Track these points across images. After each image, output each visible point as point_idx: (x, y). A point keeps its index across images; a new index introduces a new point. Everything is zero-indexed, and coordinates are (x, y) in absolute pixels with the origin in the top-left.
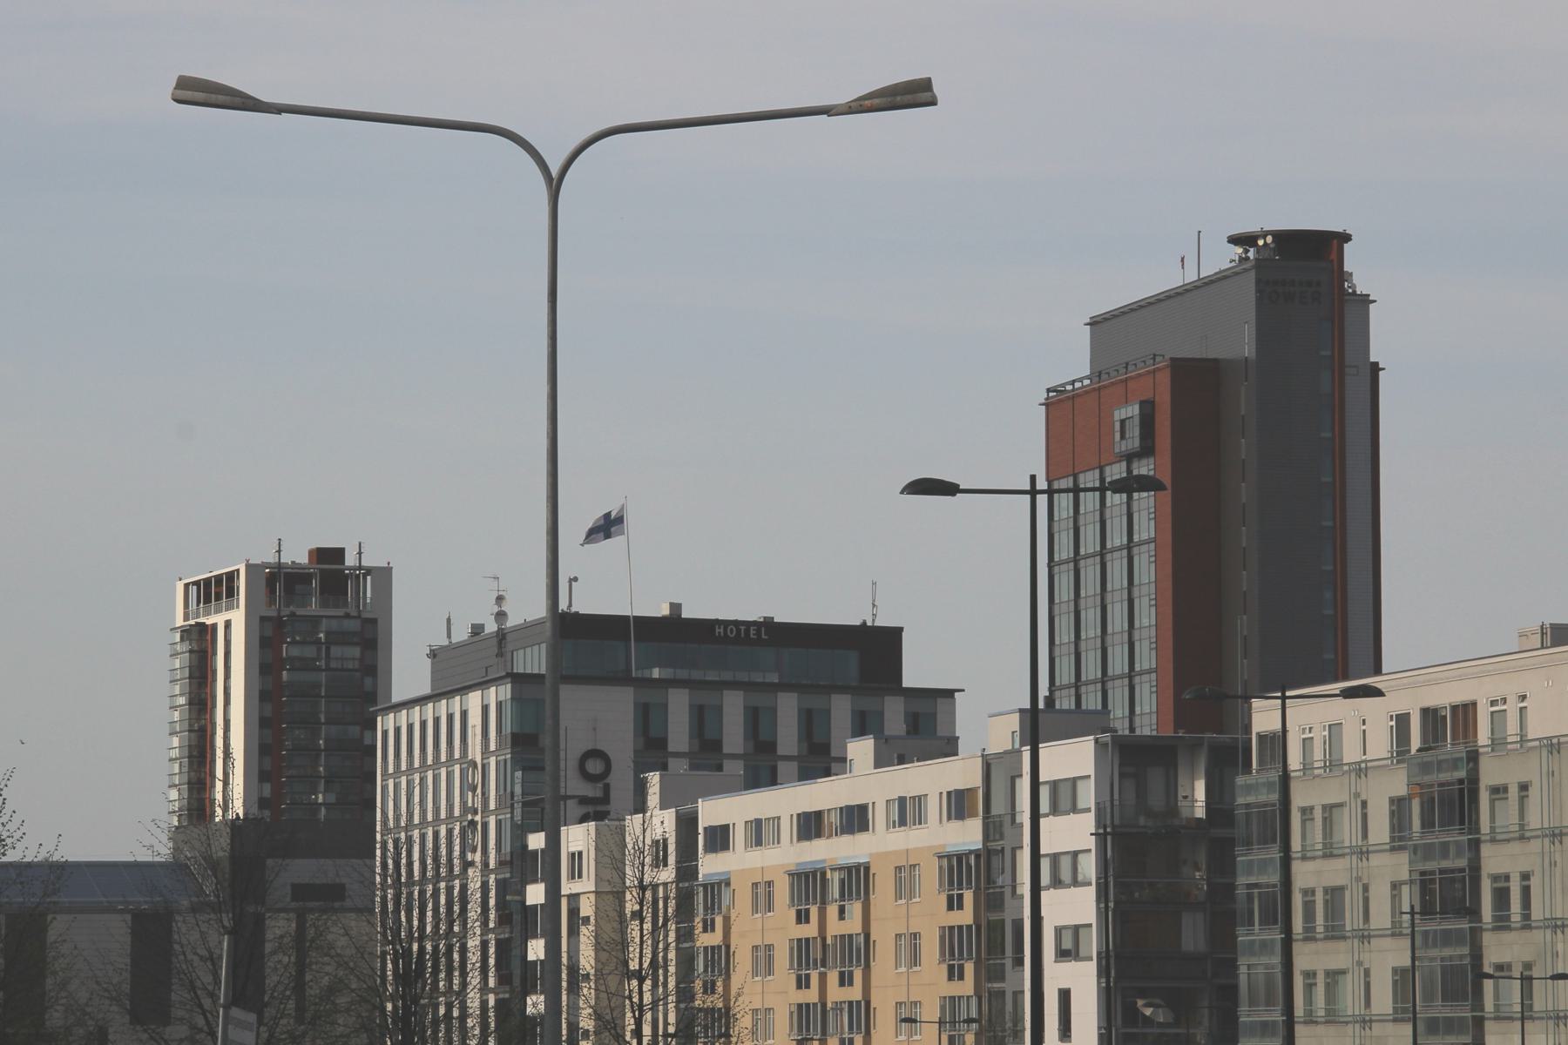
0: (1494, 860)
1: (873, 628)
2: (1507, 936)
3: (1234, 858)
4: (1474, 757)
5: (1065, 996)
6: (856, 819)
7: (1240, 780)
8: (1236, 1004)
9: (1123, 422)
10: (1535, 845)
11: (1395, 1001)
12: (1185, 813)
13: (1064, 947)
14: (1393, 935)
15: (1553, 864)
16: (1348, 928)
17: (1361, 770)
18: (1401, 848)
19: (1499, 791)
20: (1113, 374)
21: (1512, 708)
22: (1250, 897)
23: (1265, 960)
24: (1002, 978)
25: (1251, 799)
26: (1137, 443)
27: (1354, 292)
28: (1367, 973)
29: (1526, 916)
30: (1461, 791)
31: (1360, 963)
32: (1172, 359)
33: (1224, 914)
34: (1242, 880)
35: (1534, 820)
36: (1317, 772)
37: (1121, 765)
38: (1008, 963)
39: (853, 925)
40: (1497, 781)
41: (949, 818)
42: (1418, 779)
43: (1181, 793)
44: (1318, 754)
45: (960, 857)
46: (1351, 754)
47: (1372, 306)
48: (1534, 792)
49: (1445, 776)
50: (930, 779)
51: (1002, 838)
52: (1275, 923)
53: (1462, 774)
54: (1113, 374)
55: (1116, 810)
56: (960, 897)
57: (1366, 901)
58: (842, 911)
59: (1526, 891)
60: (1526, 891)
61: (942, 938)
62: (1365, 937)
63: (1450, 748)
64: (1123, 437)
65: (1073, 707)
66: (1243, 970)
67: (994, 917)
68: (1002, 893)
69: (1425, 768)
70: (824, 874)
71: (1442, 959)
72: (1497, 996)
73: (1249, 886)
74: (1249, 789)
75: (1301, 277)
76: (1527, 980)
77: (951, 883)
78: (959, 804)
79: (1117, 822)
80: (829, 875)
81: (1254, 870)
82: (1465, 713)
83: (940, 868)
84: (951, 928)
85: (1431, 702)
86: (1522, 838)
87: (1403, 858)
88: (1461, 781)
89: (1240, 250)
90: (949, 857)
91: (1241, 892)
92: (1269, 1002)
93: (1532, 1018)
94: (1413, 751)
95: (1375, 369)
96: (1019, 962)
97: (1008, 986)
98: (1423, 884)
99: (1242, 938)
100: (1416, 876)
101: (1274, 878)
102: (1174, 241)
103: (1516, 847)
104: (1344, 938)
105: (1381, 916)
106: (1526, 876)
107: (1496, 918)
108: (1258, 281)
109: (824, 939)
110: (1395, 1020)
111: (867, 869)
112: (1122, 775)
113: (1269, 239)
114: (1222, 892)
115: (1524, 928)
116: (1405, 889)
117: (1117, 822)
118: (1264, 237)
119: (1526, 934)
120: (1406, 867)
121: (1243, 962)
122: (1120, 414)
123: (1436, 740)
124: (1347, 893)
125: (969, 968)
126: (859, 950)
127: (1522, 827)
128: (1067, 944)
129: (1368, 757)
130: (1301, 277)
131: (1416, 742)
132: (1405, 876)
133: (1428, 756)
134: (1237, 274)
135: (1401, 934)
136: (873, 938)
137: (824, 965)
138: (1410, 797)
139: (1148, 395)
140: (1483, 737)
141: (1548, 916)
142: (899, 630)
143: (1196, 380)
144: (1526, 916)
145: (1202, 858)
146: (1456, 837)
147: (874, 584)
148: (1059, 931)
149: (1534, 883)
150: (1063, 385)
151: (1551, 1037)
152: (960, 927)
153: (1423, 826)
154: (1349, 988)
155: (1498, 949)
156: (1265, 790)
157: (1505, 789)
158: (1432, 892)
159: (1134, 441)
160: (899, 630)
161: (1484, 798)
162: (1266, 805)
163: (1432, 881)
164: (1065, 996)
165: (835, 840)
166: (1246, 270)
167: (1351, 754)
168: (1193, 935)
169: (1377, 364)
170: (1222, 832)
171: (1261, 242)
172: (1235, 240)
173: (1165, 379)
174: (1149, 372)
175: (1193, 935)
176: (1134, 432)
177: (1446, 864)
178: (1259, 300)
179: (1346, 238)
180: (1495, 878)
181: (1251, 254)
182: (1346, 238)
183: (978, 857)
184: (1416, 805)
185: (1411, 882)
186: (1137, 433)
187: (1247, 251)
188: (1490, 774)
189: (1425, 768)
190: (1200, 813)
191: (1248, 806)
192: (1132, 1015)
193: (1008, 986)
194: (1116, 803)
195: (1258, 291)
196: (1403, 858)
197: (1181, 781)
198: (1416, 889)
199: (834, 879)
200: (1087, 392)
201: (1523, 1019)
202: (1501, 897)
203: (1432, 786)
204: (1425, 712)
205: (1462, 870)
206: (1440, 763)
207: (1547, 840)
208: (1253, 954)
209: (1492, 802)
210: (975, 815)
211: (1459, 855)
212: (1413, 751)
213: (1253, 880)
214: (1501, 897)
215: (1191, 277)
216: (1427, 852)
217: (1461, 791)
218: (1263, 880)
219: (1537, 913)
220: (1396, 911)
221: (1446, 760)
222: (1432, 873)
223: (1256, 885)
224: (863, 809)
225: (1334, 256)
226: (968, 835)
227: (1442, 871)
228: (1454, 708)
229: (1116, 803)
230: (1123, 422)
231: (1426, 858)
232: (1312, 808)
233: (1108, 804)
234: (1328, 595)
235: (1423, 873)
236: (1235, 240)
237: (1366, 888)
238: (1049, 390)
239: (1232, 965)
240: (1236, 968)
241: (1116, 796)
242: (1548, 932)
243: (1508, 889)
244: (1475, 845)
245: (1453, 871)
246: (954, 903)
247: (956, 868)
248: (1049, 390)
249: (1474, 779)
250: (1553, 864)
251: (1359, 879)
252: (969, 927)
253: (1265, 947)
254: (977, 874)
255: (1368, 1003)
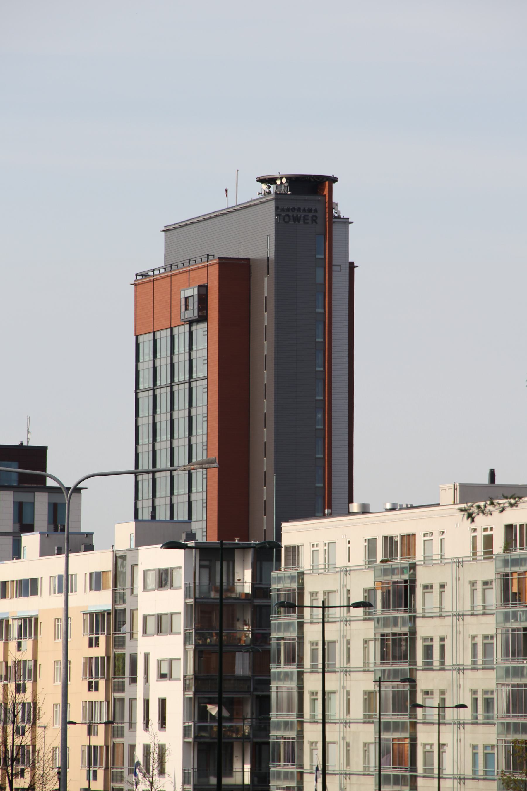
0: (425, 629)
1: (28, 447)
2: (430, 674)
3: (270, 621)
4: (413, 567)
5: (163, 703)
6: (29, 587)
7: (274, 574)
8: (268, 710)
9: (186, 299)
10: (448, 620)
11: (365, 711)
12: (238, 590)
13: (162, 672)
14: (364, 671)
15: (458, 632)
16: (337, 666)
17: (347, 571)
18: (369, 619)
19: (427, 587)
20: (180, 266)
21: (436, 538)
22: (279, 645)
23: (287, 684)
24: (123, 690)
25: (280, 586)
26: (196, 314)
27: (339, 216)
28: (348, 693)
29: (442, 663)
30: (406, 587)
31: (344, 687)
32: (219, 258)
33: (262, 654)
34: (274, 635)
35: (448, 607)
36: (320, 571)
37: (200, 560)
38: (127, 681)
39: (27, 655)
40: (427, 582)
41: (91, 589)
42: (381, 579)
43: (237, 577)
44: (321, 560)
45: (97, 614)
46: (341, 561)
47: (350, 226)
48: (448, 589)
49: (397, 578)
50: (83, 564)
51: (124, 602)
52: (294, 661)
53: (406, 577)
54: (180, 266)
55: (197, 588)
56: (97, 639)
57: (349, 650)
58: (19, 645)
59: (442, 647)
60: (442, 647)
61: (85, 664)
62: (347, 672)
63: (399, 562)
64: (186, 309)
65: (168, 518)
66: (273, 690)
67: (119, 651)
68: (124, 637)
69: (385, 572)
70: (7, 621)
71: (393, 687)
72: (424, 604)
73: (279, 639)
74: (279, 579)
75: (305, 203)
76: (442, 707)
77: (91, 630)
78: (96, 581)
79: (197, 596)
80: (11, 622)
81: (281, 628)
82: (409, 540)
83: (84, 620)
84: (91, 658)
85: (389, 534)
86: (441, 616)
87: (371, 625)
88: (406, 581)
89: (264, 186)
90: (91, 614)
91: (273, 642)
92: (289, 710)
93: (444, 724)
94: (378, 562)
95: (352, 266)
96: (134, 680)
97: (126, 695)
98: (382, 640)
99: (274, 669)
100: (379, 637)
101: (293, 634)
102: (224, 176)
103: (437, 621)
104: (335, 672)
105: (357, 661)
106: (442, 639)
107: (426, 664)
108: (277, 208)
109: (7, 663)
110: (364, 723)
111: (36, 619)
112: (200, 566)
113: (284, 180)
114: (261, 637)
115: (441, 670)
116: (372, 644)
117: (197, 596)
118: (281, 179)
119: (442, 673)
120: (372, 631)
121: (274, 685)
122: (185, 294)
123: (391, 555)
124: (337, 645)
125: (102, 684)
126: (30, 671)
127: (441, 609)
128: (165, 670)
129: (351, 564)
130: (305, 203)
131: (380, 556)
132: (372, 636)
133: (387, 565)
134: (262, 203)
135: (369, 671)
136: (39, 663)
137: (6, 679)
138: (375, 589)
139: (203, 282)
140: (419, 556)
141: (455, 663)
142: (45, 448)
143: (235, 273)
144: (442, 663)
145: (249, 618)
146: (402, 614)
147: (29, 418)
148: (159, 663)
149: (448, 643)
150: (147, 272)
151: (455, 735)
152: (97, 658)
153: (383, 607)
154: (337, 702)
155: (425, 681)
156: (289, 581)
157: (432, 587)
158: (387, 646)
159: (194, 312)
160: (45, 448)
161: (419, 591)
162: (289, 590)
163: (387, 640)
164: (163, 703)
165: (15, 600)
166: (269, 201)
167: (341, 561)
168: (242, 666)
169: (352, 263)
170: (261, 604)
171: (278, 182)
172: (262, 180)
173: (215, 271)
174: (204, 267)
175: (242, 666)
176: (194, 305)
177: (397, 630)
178: (277, 223)
179: (334, 180)
180: (425, 639)
181: (273, 189)
182: (334, 180)
183: (109, 614)
184: (379, 593)
185: (376, 640)
186: (196, 306)
187: (270, 187)
188: (421, 579)
189: (385, 572)
190: (248, 589)
191: (278, 590)
192: (203, 714)
193: (126, 695)
194: (197, 584)
195: (277, 215)
196: (371, 625)
197: (236, 570)
198: (379, 643)
199: (15, 626)
200: (163, 278)
201: (439, 724)
202: (428, 651)
203: (389, 583)
204: (385, 538)
205: (405, 634)
206: (393, 569)
207: (455, 618)
208: (279, 680)
209: (424, 594)
210: (109, 588)
211: (404, 624)
212: (378, 562)
213: (281, 635)
214: (428, 651)
215: (232, 203)
216: (385, 622)
217: (406, 587)
218: (287, 635)
219: (448, 661)
220: (366, 656)
221: (397, 568)
222: (387, 635)
223: (283, 638)
224: (35, 581)
225: (326, 192)
226: (103, 601)
227: (394, 634)
228: (403, 537)
229: (197, 584)
230: (186, 299)
231: (385, 625)
232: (317, 593)
233: (192, 585)
234: (320, 416)
235: (382, 635)
236: (262, 180)
237: (348, 643)
238: (137, 275)
239: (267, 683)
240: (269, 688)
241: (197, 580)
242: (455, 672)
243: (432, 646)
244: (413, 619)
245: (400, 634)
246: (93, 643)
247: (96, 621)
248: (137, 275)
249: (413, 581)
250: (458, 632)
251: (344, 636)
252: (103, 658)
253: (287, 676)
254: (111, 624)
255: (348, 712)
